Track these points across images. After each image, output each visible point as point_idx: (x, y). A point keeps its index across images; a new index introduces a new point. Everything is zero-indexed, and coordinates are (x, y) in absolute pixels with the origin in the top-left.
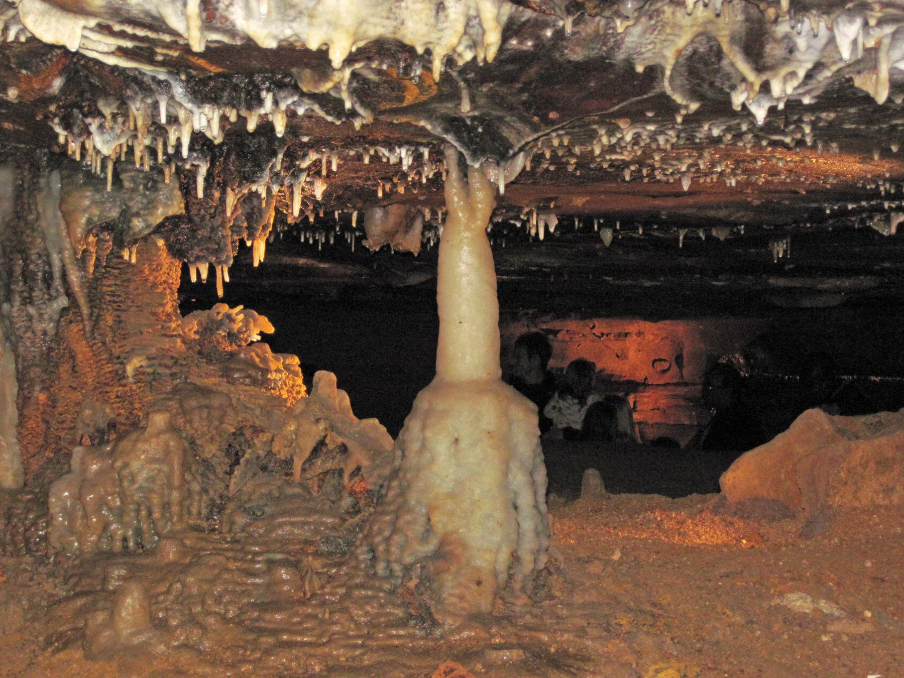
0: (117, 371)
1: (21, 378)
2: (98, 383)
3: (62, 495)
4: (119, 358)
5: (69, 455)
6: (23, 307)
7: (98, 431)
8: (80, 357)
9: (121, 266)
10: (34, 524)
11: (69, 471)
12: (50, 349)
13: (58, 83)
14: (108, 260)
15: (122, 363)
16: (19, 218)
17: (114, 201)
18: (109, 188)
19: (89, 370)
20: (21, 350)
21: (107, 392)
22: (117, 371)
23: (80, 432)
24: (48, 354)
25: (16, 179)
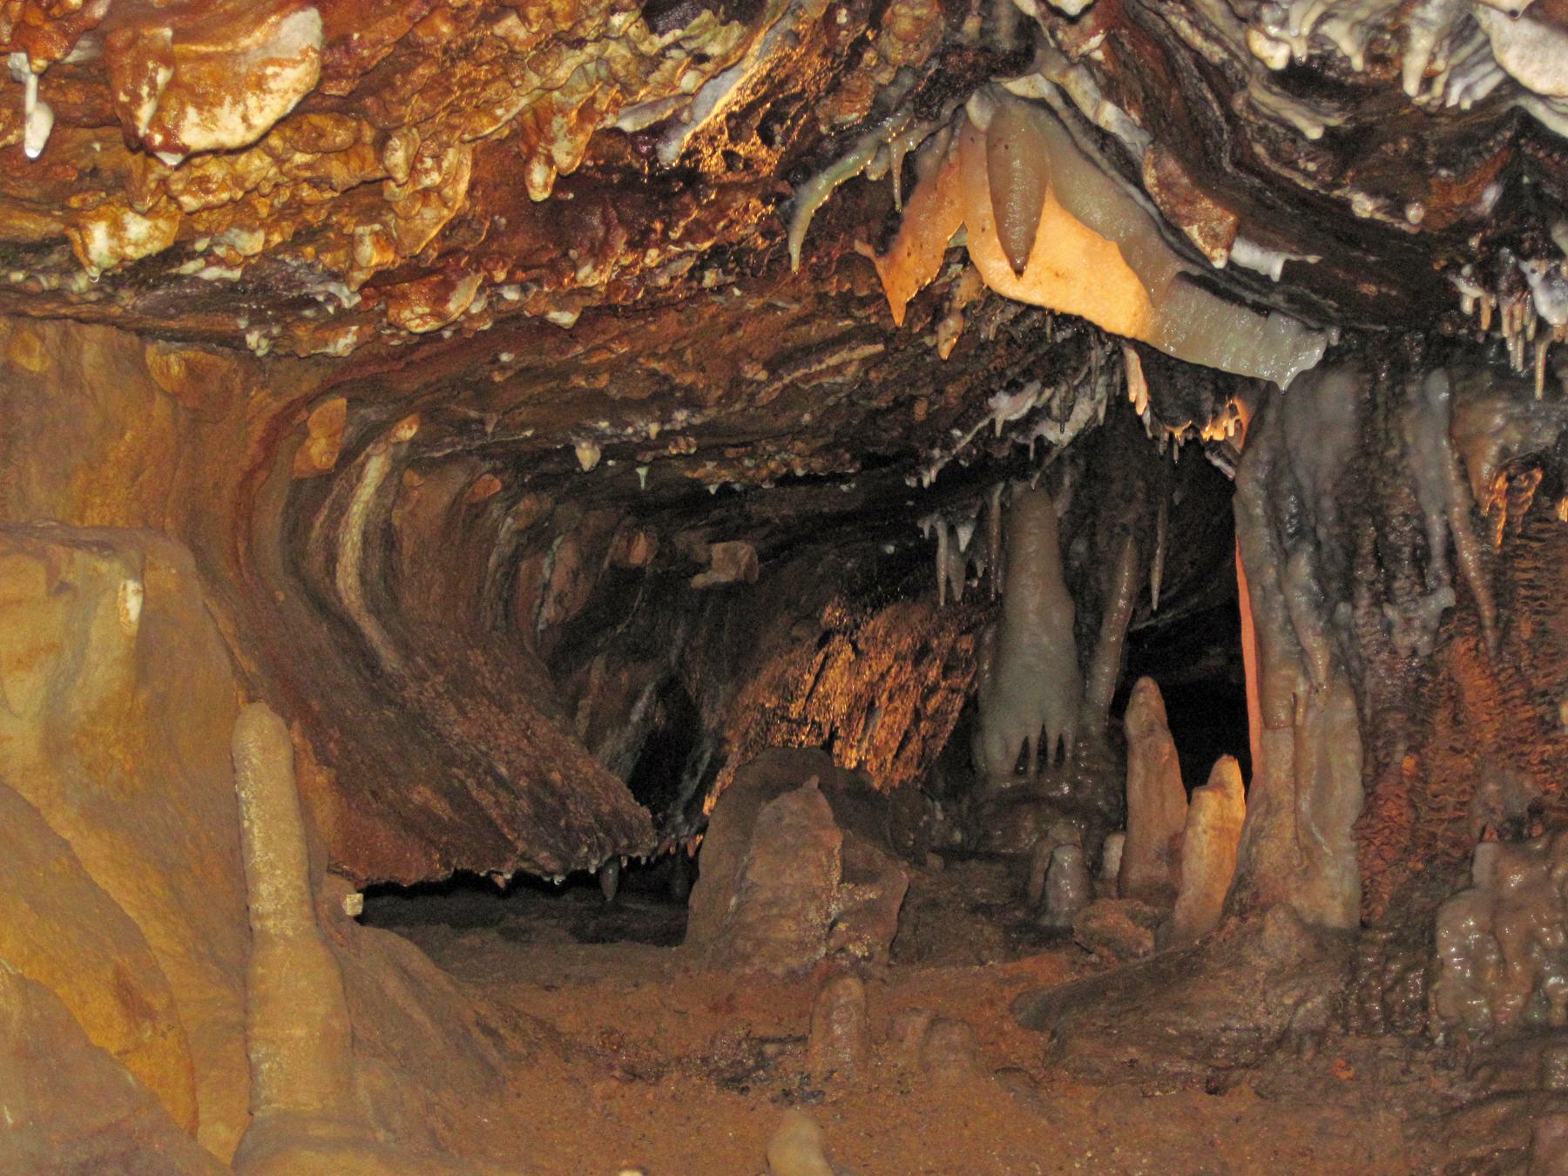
0: (1542, 717)
1: (1371, 734)
2: (1504, 739)
3: (1459, 931)
4: (1544, 694)
5: (1469, 858)
6: (1375, 610)
7: (1512, 820)
8: (1470, 696)
9: (1546, 536)
10: (1400, 979)
11: (1470, 885)
12: (1420, 681)
13: (1491, 195)
14: (1526, 525)
15: (1551, 703)
16: (1368, 455)
17: (1547, 418)
18: (1539, 392)
19: (1486, 718)
20: (1370, 683)
21: (1522, 754)
22: (1542, 717)
23: (1480, 823)
24: (1416, 690)
25: (1362, 390)
